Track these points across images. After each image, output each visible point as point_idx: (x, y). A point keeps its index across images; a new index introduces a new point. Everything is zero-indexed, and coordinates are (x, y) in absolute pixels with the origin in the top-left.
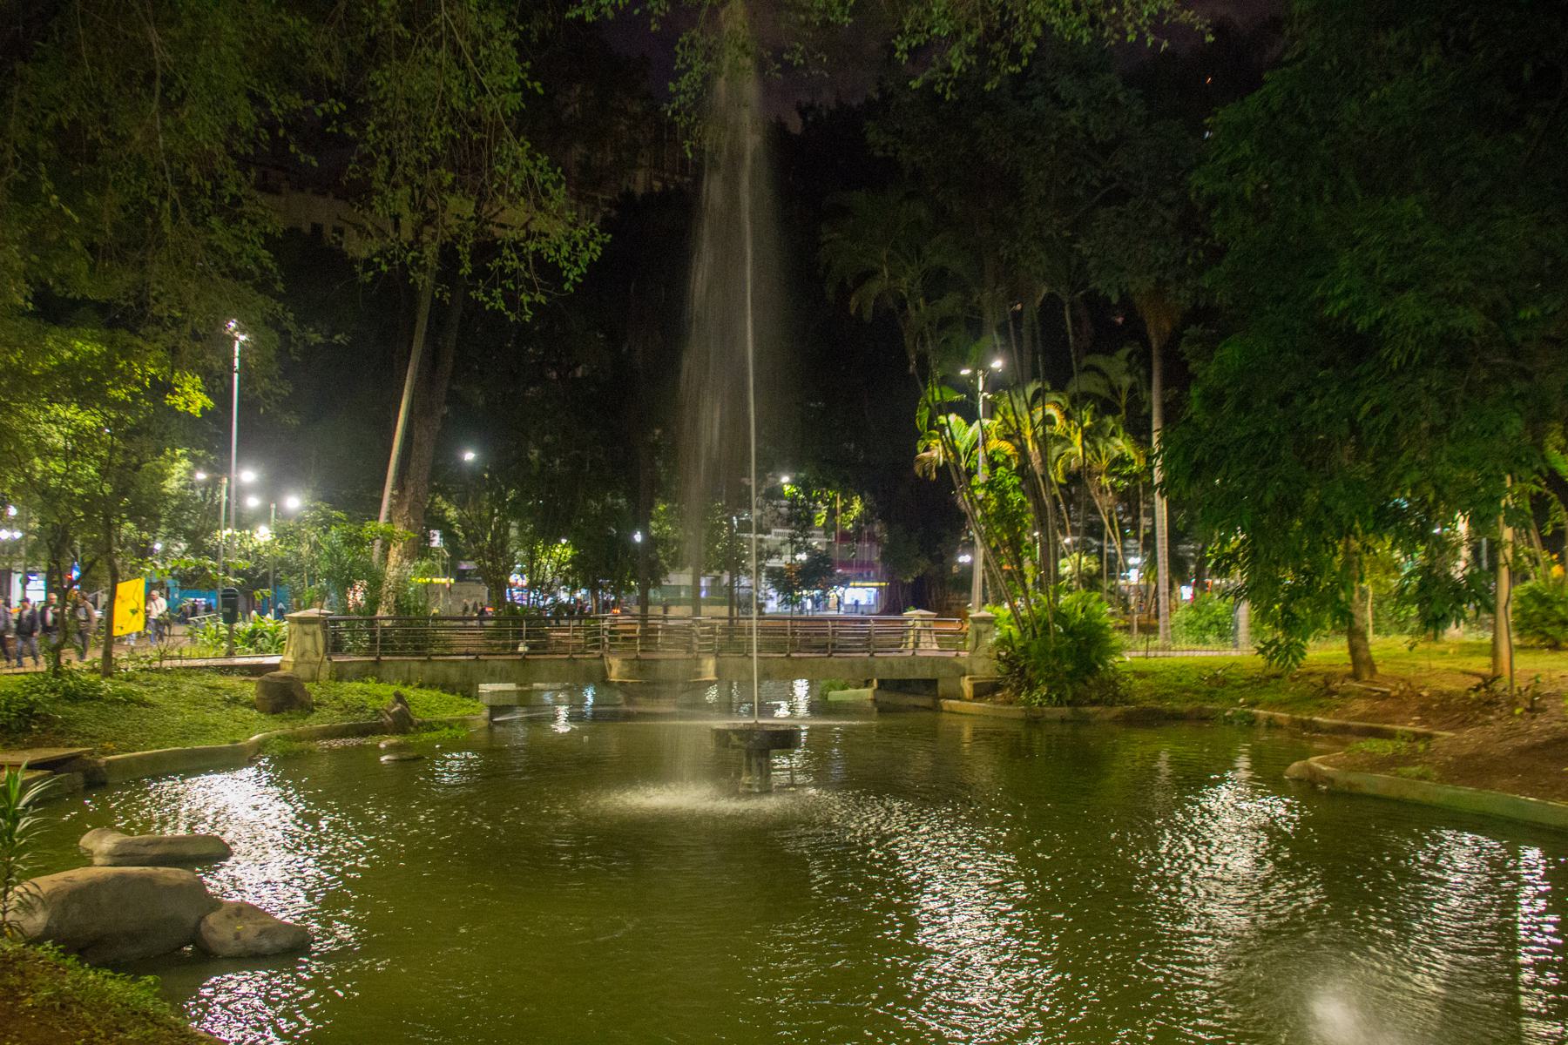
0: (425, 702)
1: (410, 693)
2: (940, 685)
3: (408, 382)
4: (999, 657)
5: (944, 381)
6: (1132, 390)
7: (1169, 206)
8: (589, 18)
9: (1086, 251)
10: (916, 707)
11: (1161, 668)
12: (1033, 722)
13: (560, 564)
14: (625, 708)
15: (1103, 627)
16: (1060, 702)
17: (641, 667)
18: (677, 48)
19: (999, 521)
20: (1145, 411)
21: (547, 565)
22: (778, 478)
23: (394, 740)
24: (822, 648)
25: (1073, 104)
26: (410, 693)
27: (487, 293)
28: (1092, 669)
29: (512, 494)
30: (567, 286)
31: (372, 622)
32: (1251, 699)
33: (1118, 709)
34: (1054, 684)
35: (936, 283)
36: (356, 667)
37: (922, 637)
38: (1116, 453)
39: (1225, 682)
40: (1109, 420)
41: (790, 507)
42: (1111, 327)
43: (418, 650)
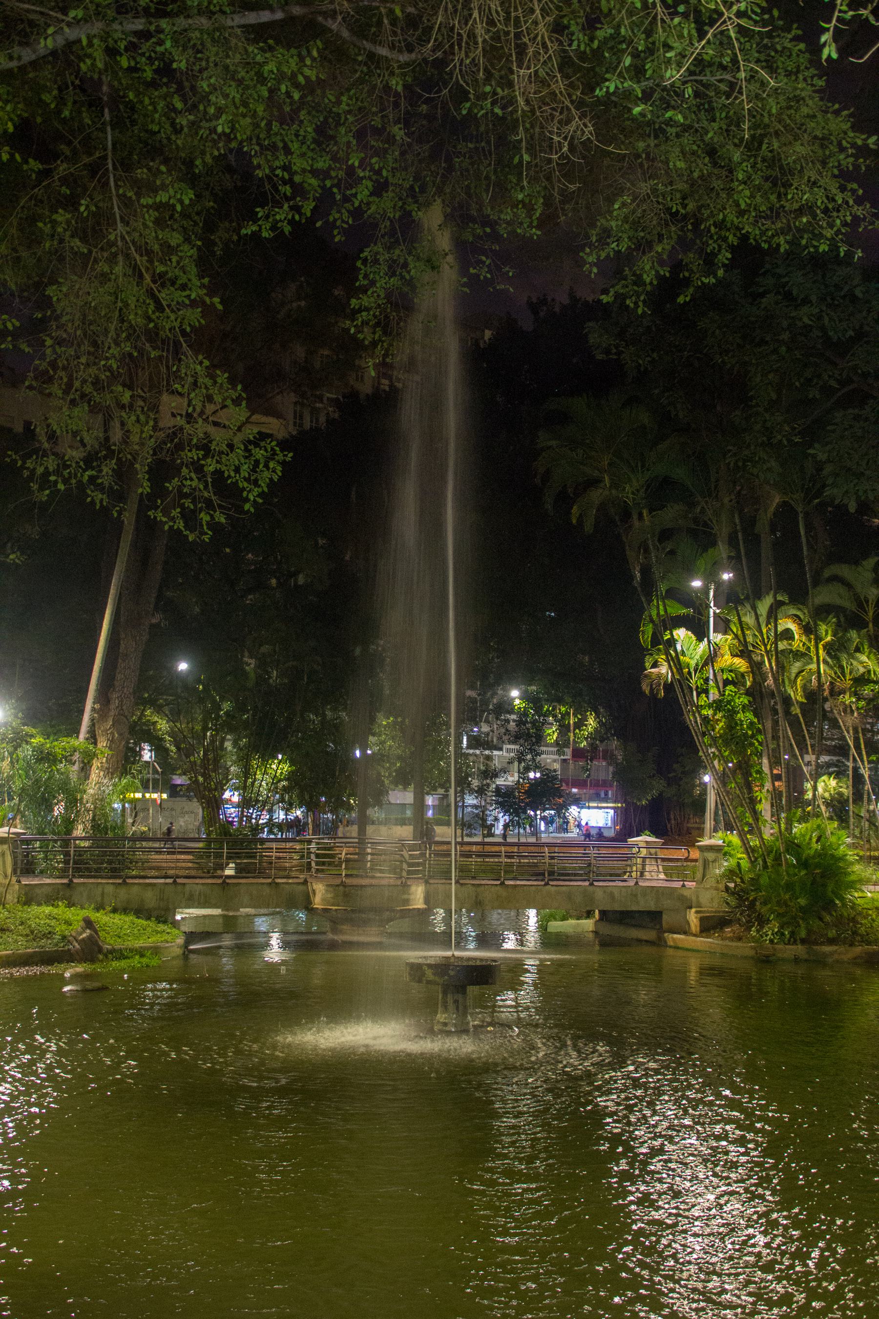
0: (116, 927)
1: (101, 918)
2: (665, 917)
3: (113, 591)
4: (727, 889)
5: (671, 594)
8: (265, 234)
9: (822, 457)
10: (639, 941)
12: (765, 961)
13: (276, 781)
14: (330, 936)
15: (842, 858)
16: (793, 940)
17: (345, 892)
18: (359, 264)
19: (727, 743)
21: (263, 782)
22: (507, 691)
23: (80, 969)
24: (539, 875)
25: (806, 301)
26: (101, 918)
27: (166, 513)
28: (829, 906)
29: (226, 706)
31: (66, 843)
33: (858, 950)
35: (661, 491)
36: (44, 890)
37: (649, 865)
38: (862, 670)
40: (853, 634)
41: (520, 723)
43: (114, 873)
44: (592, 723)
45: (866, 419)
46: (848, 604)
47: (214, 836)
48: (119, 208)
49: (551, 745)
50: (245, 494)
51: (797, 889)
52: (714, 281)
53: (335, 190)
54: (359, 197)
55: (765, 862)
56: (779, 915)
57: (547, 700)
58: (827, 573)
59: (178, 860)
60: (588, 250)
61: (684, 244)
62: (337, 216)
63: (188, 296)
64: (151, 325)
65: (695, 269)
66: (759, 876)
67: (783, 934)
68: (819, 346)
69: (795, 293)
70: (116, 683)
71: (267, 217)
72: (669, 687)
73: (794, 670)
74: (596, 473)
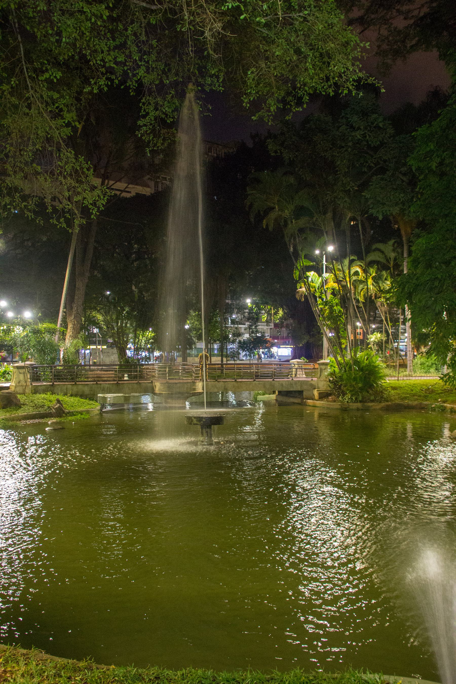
0: (71, 402)
2: (304, 393)
4: (330, 380)
6: (395, 259)
7: (404, 175)
9: (368, 196)
10: (294, 403)
11: (404, 385)
12: (344, 410)
16: (356, 401)
20: (401, 268)
23: (54, 420)
25: (359, 128)
27: (58, 220)
28: (371, 386)
30: (92, 217)
32: (444, 399)
33: (383, 404)
34: (354, 393)
35: (300, 212)
39: (432, 391)
40: (384, 273)
41: (249, 313)
42: (384, 230)
43: (73, 380)
44: (281, 312)
45: (386, 180)
46: (383, 260)
47: (122, 363)
48: (30, 83)
49: (264, 322)
50: (91, 211)
51: (358, 380)
52: (301, 110)
53: (129, 71)
54: (140, 74)
55: (345, 369)
56: (351, 391)
57: (262, 304)
58: (374, 247)
59: (109, 374)
60: (244, 96)
61: (288, 94)
62: (131, 83)
63: (64, 122)
64: (49, 136)
65: (292, 104)
66: (343, 375)
67: (352, 399)
68: (365, 149)
69: (354, 125)
70: (75, 300)
71: (95, 83)
72: (306, 297)
73: (360, 288)
74: (272, 205)
